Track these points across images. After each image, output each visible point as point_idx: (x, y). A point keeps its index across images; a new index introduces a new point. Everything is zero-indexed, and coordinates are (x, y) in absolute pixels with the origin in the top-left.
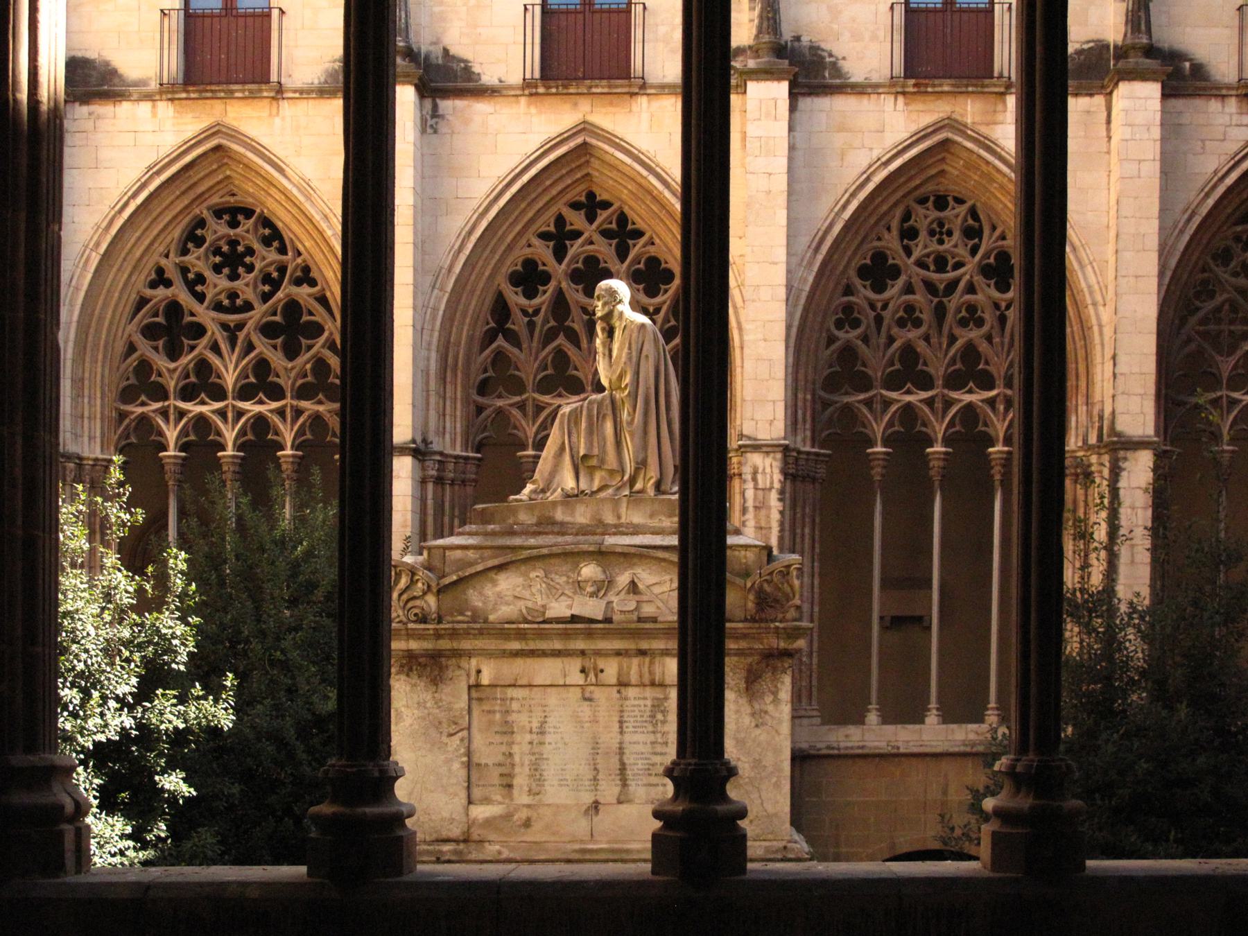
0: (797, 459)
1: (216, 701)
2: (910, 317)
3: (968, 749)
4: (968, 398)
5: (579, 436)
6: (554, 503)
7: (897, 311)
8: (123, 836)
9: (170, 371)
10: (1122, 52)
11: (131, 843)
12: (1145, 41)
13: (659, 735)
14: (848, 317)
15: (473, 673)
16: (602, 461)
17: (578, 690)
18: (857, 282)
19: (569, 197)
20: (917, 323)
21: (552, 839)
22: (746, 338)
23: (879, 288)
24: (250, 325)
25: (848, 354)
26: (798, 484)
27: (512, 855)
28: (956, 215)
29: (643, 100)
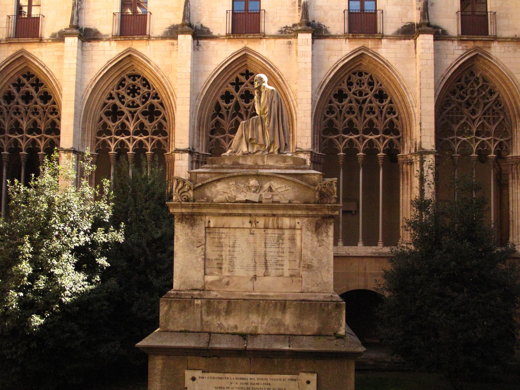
0: (315, 156)
1: (118, 232)
2: (351, 111)
3: (373, 255)
4: (370, 137)
5: (248, 131)
6: (239, 156)
7: (347, 109)
8: (83, 281)
9: (113, 126)
10: (419, 26)
11: (86, 283)
12: (427, 21)
13: (280, 249)
14: (331, 111)
15: (207, 222)
16: (257, 141)
17: (248, 230)
18: (333, 99)
19: (240, 71)
20: (353, 113)
21: (238, 290)
22: (298, 115)
23: (341, 101)
24: (138, 112)
25: (331, 123)
26: (315, 165)
27: (222, 297)
28: (365, 78)
29: (264, 40)
